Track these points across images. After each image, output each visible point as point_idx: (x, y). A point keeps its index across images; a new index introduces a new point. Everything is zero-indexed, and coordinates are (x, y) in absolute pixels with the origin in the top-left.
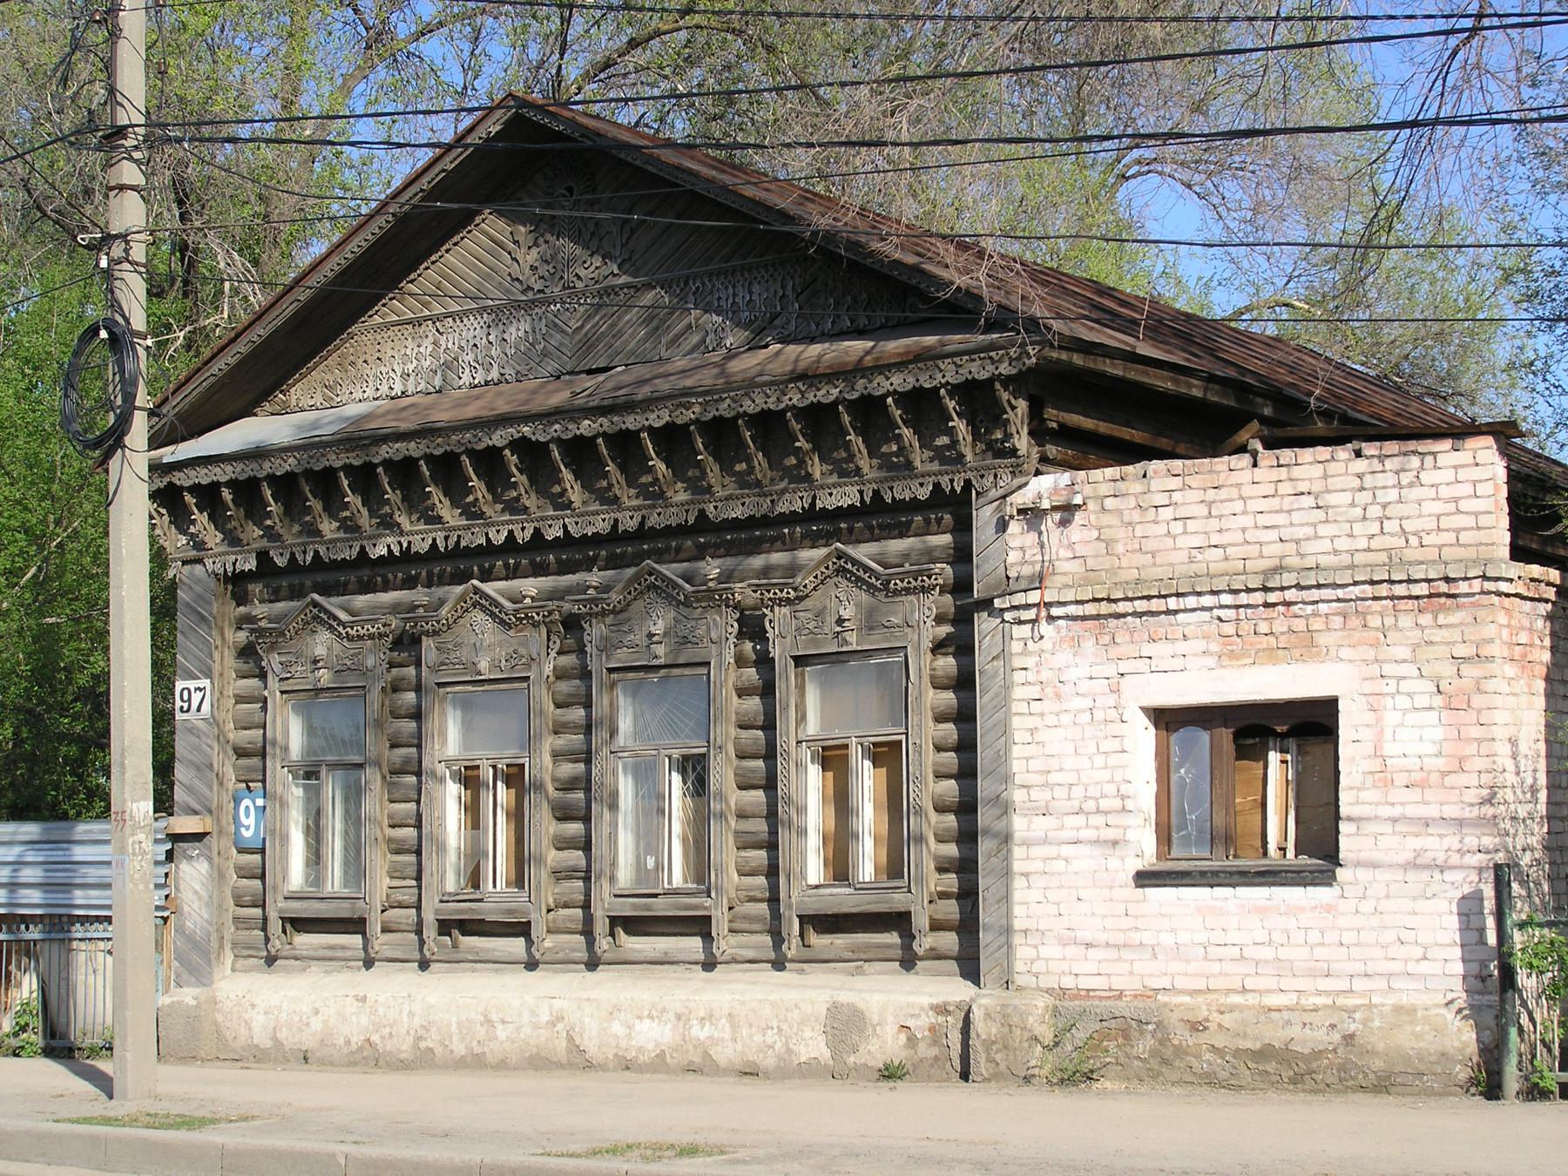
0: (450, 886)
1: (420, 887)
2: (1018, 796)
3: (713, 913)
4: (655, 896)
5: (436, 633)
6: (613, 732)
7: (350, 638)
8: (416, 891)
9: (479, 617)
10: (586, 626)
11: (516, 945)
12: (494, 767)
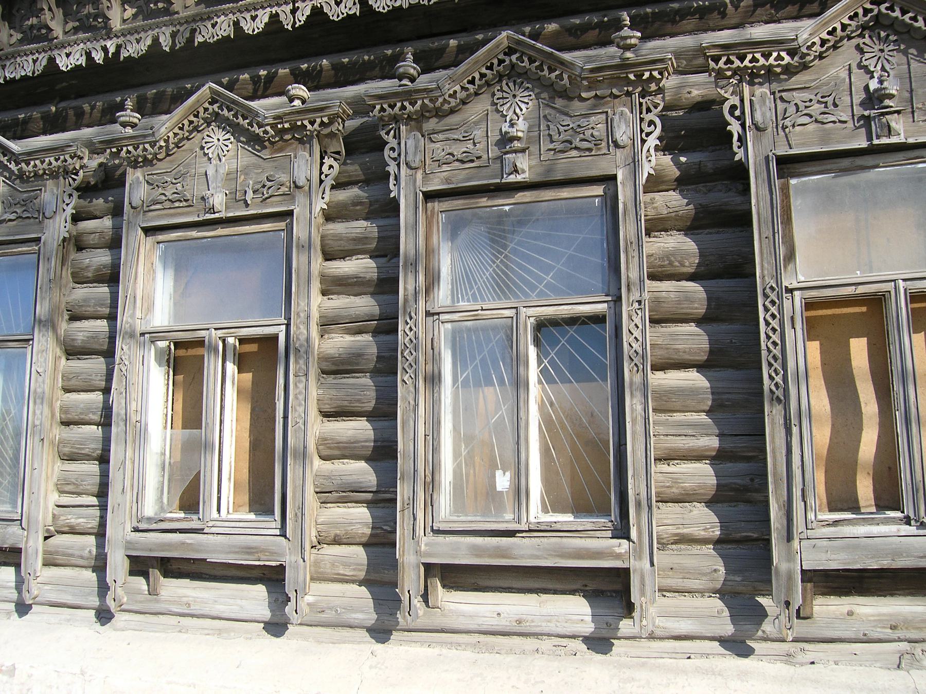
0: (149, 509)
1: (103, 507)
2: (710, 396)
3: (633, 564)
4: (511, 534)
5: (147, 162)
6: (432, 281)
7: (21, 176)
8: (97, 512)
9: (217, 138)
10: (390, 138)
11: (254, 600)
12: (224, 341)
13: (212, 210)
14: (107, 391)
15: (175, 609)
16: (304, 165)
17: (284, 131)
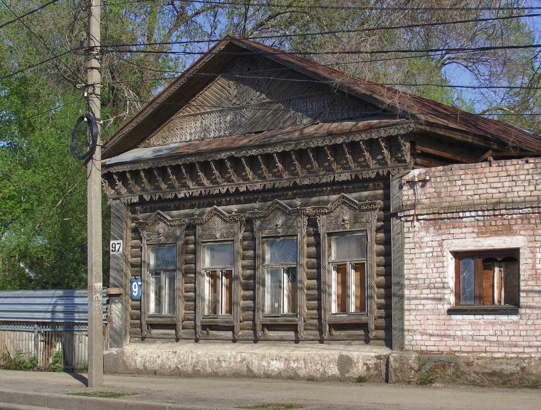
0: (206, 313)
1: (195, 313)
4: (278, 317)
7: (171, 226)
12: (222, 271)
13: (216, 238)
14: (195, 283)
15: (213, 338)
16: (236, 226)
17: (231, 219)
